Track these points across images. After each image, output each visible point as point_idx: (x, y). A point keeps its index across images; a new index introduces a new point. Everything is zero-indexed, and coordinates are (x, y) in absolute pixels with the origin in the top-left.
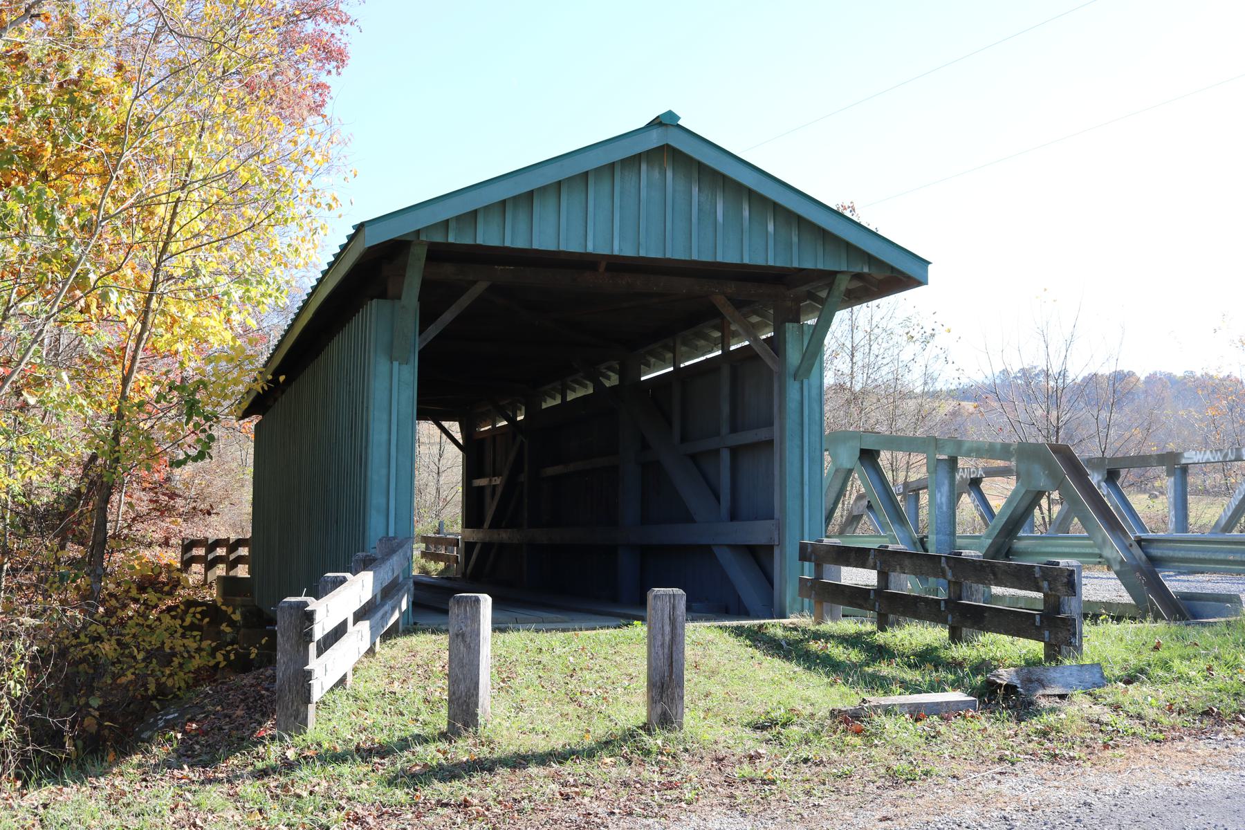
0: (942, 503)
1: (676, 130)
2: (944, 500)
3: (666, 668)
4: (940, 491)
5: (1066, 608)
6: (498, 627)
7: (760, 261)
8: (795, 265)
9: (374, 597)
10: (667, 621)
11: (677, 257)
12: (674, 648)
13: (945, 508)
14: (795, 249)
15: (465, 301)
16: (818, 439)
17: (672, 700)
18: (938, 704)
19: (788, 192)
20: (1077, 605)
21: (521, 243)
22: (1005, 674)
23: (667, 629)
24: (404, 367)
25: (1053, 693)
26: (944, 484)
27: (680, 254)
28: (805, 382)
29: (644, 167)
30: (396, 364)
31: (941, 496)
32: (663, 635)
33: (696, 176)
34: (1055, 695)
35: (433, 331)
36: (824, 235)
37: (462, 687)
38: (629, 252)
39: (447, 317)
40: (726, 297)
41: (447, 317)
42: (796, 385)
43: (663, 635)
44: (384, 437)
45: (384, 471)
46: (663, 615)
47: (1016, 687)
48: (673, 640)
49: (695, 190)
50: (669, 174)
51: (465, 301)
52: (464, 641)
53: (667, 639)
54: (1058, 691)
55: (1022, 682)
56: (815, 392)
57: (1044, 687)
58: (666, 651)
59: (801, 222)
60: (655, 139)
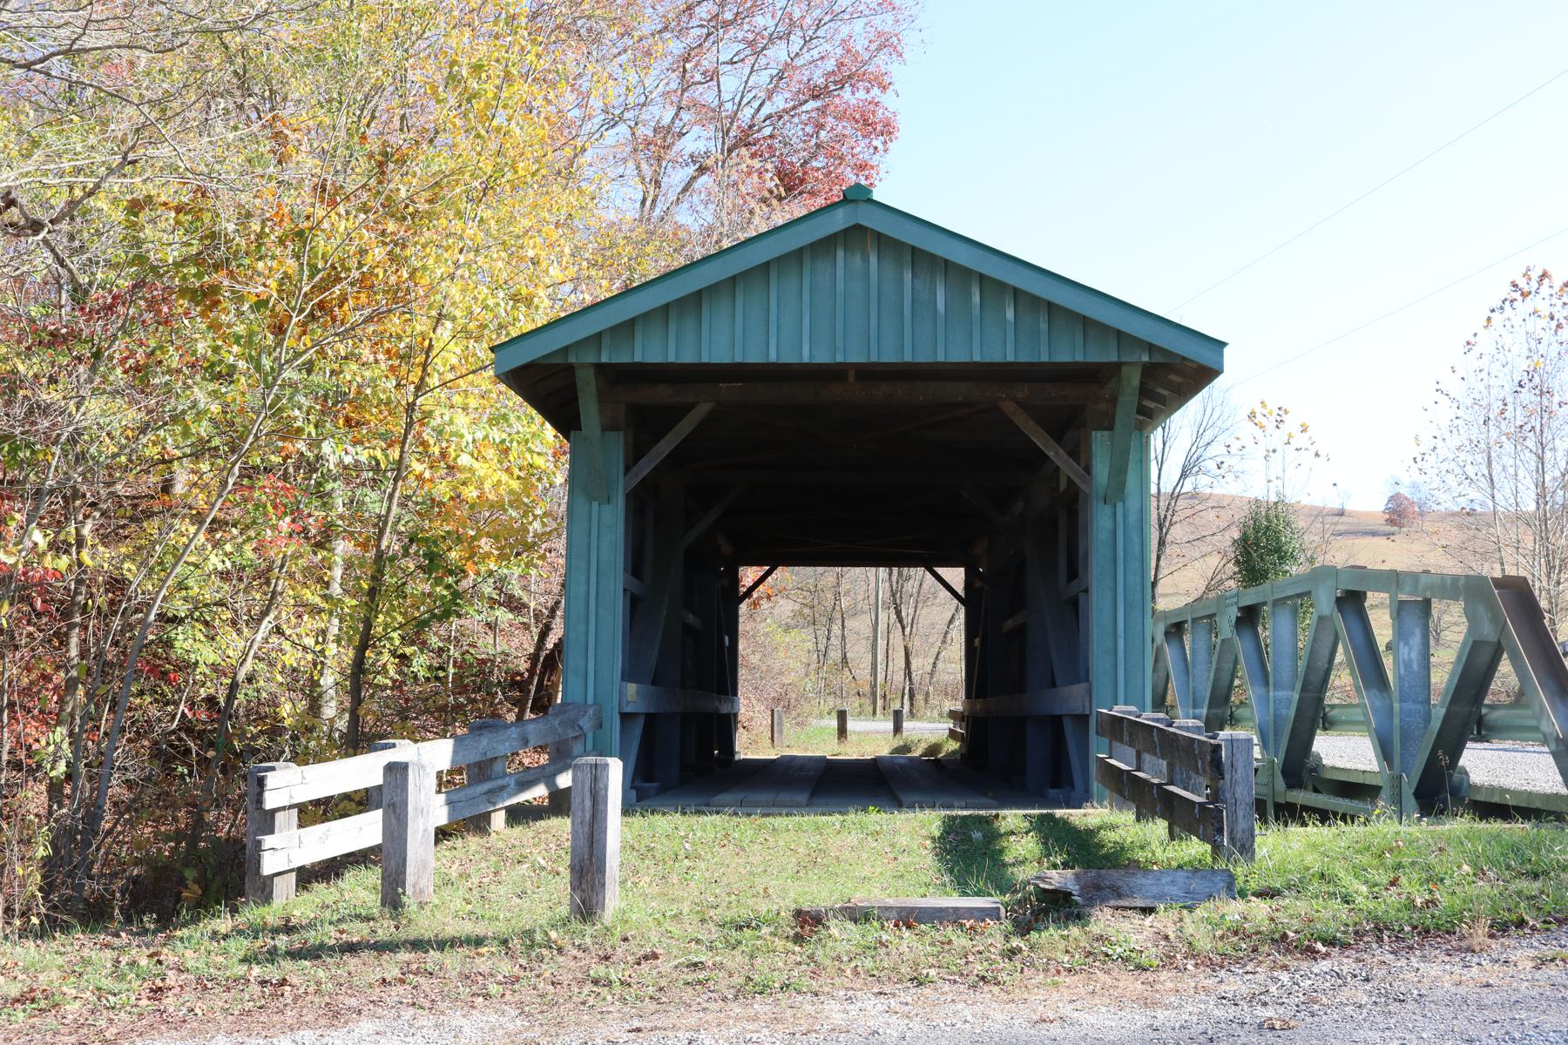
0: (1411, 660)
1: (868, 206)
2: (1414, 655)
3: (586, 850)
4: (1407, 644)
5: (1228, 795)
6: (627, 811)
7: (996, 357)
8: (1045, 358)
9: (1476, 788)
10: (588, 794)
11: (885, 359)
12: (596, 827)
13: (1415, 666)
14: (1044, 338)
15: (684, 428)
16: (1138, 579)
17: (592, 887)
18: (941, 910)
19: (1021, 269)
20: (1245, 792)
21: (688, 358)
22: (1057, 876)
23: (588, 804)
24: (606, 508)
25: (1134, 905)
26: (1413, 633)
27: (889, 357)
28: (1119, 505)
29: (840, 254)
30: (595, 504)
31: (1410, 650)
32: (583, 811)
33: (909, 259)
34: (1135, 908)
35: (645, 467)
36: (1087, 324)
37: (393, 863)
38: (822, 357)
39: (664, 448)
40: (1017, 403)
41: (664, 448)
42: (1108, 510)
43: (583, 811)
44: (583, 588)
45: (582, 628)
46: (583, 787)
47: (1070, 894)
48: (594, 816)
49: (908, 276)
50: (873, 259)
51: (684, 428)
52: (395, 812)
53: (588, 815)
54: (1140, 903)
55: (1082, 888)
56: (1133, 518)
57: (1120, 896)
58: (586, 829)
59: (1053, 309)
60: (840, 220)
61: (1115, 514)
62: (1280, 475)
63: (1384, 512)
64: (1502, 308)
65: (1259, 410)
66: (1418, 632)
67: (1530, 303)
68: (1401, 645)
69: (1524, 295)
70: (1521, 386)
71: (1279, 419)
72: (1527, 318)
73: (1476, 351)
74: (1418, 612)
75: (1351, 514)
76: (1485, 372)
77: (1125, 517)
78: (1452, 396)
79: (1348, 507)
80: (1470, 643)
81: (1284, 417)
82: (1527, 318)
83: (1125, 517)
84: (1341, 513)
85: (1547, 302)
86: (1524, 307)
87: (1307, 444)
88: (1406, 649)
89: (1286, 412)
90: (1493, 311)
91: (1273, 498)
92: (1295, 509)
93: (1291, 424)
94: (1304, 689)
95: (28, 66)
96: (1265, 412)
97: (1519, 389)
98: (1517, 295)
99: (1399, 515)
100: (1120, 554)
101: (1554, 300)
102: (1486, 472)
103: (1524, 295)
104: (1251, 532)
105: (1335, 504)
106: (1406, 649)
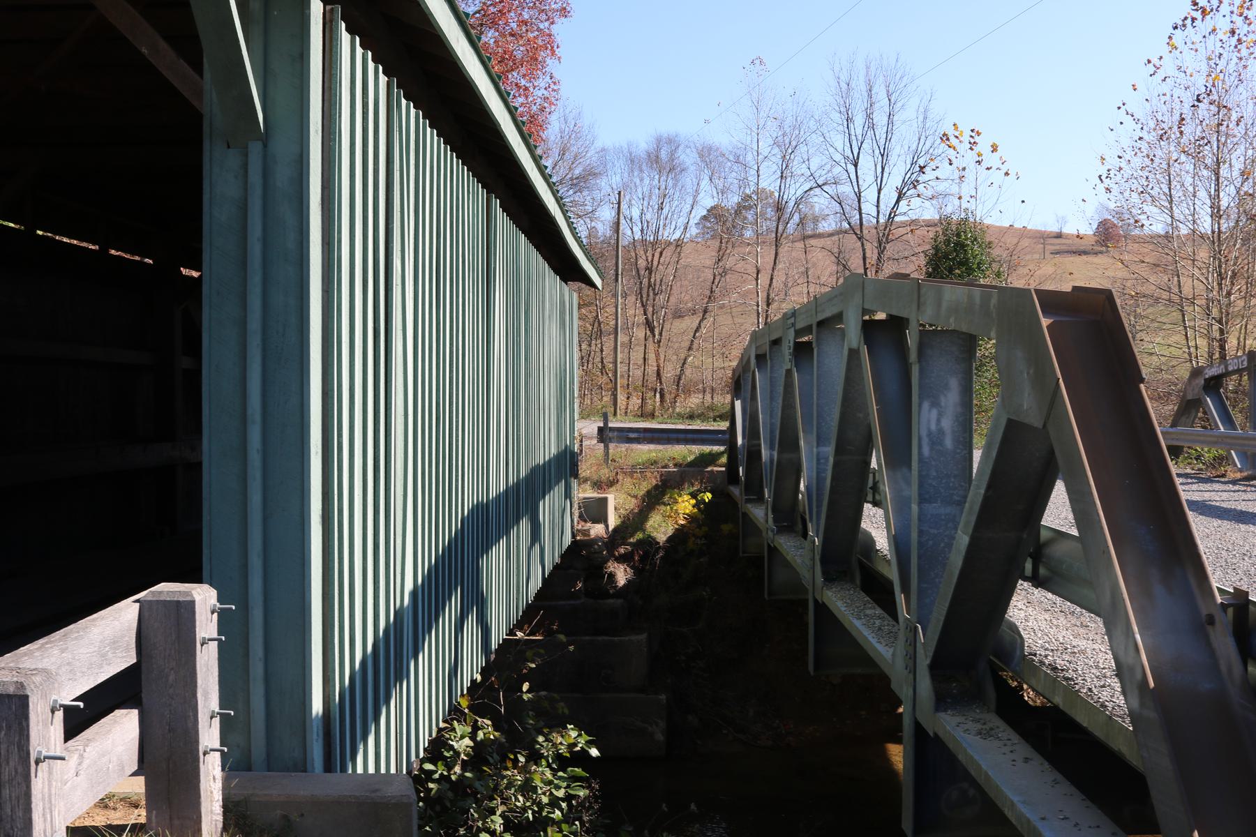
0: (941, 432)
2: (947, 424)
4: (935, 404)
13: (949, 443)
31: (940, 415)
61: (245, 167)
62: (974, 194)
63: (1094, 235)
64: (1184, 26)
65: (951, 132)
66: (954, 383)
67: (1209, 22)
68: (926, 405)
69: (1204, 12)
70: (1198, 100)
71: (972, 141)
72: (1207, 35)
73: (1161, 74)
75: (1068, 237)
76: (1168, 95)
77: (266, 174)
78: (1136, 116)
80: (1003, 422)
81: (977, 139)
82: (1207, 35)
83: (266, 174)
84: (1059, 235)
85: (1228, 19)
86: (1204, 26)
87: (997, 163)
88: (934, 413)
89: (978, 134)
90: (1175, 28)
92: (984, 229)
93: (984, 145)
96: (957, 134)
97: (1196, 103)
98: (1198, 15)
99: (1107, 235)
100: (255, 249)
101: (1235, 17)
102: (1167, 191)
103: (1204, 12)
105: (1053, 228)
106: (934, 413)
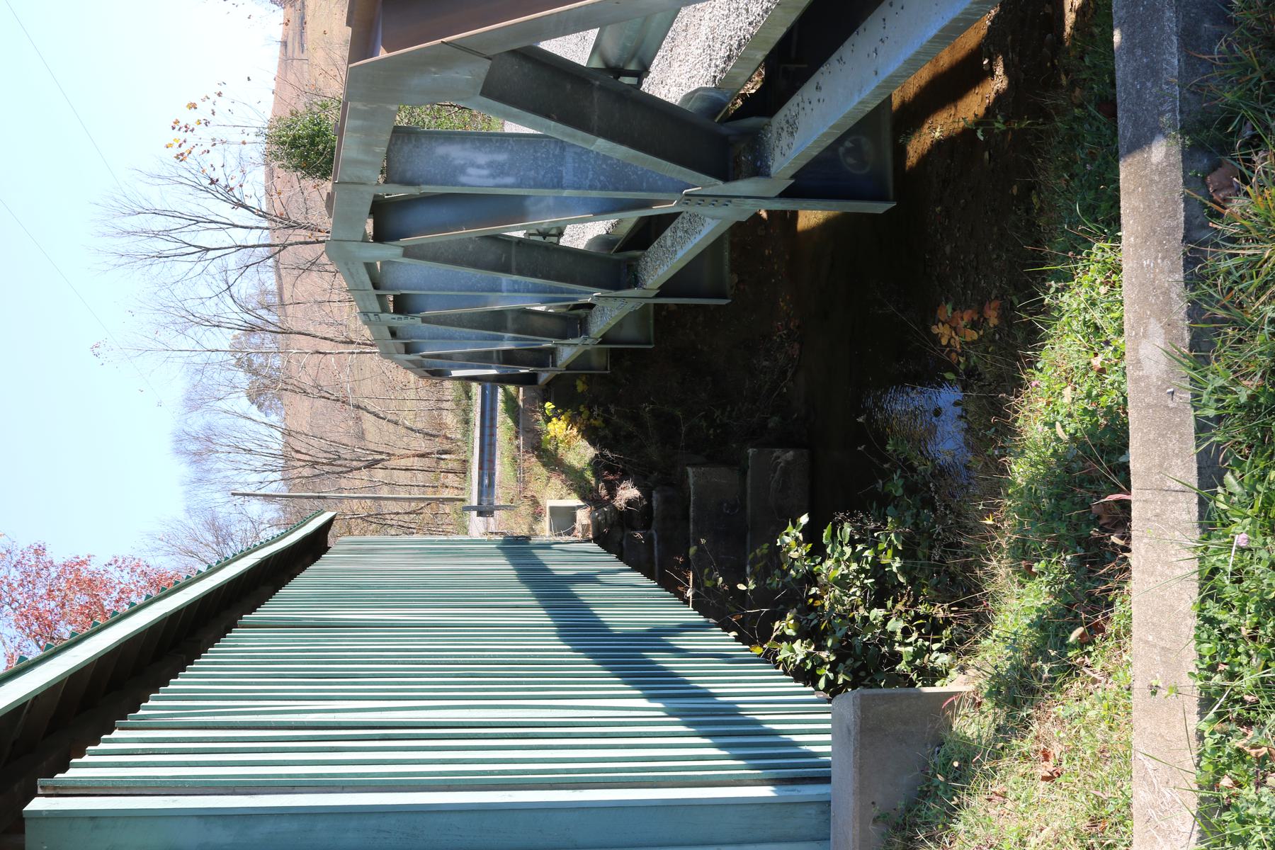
0: (490, 165)
2: (482, 158)
4: (462, 170)
13: (502, 157)
26: (445, 158)
31: (473, 165)
66: (440, 150)
68: (463, 179)
71: (184, 129)
74: (406, 149)
79: (279, 37)
81: (182, 124)
87: (209, 104)
88: (471, 171)
89: (177, 122)
91: (262, 139)
93: (189, 118)
94: (506, 269)
95: (248, 267)
104: (295, 161)
105: (276, 50)
